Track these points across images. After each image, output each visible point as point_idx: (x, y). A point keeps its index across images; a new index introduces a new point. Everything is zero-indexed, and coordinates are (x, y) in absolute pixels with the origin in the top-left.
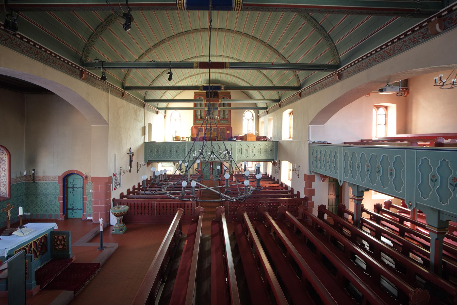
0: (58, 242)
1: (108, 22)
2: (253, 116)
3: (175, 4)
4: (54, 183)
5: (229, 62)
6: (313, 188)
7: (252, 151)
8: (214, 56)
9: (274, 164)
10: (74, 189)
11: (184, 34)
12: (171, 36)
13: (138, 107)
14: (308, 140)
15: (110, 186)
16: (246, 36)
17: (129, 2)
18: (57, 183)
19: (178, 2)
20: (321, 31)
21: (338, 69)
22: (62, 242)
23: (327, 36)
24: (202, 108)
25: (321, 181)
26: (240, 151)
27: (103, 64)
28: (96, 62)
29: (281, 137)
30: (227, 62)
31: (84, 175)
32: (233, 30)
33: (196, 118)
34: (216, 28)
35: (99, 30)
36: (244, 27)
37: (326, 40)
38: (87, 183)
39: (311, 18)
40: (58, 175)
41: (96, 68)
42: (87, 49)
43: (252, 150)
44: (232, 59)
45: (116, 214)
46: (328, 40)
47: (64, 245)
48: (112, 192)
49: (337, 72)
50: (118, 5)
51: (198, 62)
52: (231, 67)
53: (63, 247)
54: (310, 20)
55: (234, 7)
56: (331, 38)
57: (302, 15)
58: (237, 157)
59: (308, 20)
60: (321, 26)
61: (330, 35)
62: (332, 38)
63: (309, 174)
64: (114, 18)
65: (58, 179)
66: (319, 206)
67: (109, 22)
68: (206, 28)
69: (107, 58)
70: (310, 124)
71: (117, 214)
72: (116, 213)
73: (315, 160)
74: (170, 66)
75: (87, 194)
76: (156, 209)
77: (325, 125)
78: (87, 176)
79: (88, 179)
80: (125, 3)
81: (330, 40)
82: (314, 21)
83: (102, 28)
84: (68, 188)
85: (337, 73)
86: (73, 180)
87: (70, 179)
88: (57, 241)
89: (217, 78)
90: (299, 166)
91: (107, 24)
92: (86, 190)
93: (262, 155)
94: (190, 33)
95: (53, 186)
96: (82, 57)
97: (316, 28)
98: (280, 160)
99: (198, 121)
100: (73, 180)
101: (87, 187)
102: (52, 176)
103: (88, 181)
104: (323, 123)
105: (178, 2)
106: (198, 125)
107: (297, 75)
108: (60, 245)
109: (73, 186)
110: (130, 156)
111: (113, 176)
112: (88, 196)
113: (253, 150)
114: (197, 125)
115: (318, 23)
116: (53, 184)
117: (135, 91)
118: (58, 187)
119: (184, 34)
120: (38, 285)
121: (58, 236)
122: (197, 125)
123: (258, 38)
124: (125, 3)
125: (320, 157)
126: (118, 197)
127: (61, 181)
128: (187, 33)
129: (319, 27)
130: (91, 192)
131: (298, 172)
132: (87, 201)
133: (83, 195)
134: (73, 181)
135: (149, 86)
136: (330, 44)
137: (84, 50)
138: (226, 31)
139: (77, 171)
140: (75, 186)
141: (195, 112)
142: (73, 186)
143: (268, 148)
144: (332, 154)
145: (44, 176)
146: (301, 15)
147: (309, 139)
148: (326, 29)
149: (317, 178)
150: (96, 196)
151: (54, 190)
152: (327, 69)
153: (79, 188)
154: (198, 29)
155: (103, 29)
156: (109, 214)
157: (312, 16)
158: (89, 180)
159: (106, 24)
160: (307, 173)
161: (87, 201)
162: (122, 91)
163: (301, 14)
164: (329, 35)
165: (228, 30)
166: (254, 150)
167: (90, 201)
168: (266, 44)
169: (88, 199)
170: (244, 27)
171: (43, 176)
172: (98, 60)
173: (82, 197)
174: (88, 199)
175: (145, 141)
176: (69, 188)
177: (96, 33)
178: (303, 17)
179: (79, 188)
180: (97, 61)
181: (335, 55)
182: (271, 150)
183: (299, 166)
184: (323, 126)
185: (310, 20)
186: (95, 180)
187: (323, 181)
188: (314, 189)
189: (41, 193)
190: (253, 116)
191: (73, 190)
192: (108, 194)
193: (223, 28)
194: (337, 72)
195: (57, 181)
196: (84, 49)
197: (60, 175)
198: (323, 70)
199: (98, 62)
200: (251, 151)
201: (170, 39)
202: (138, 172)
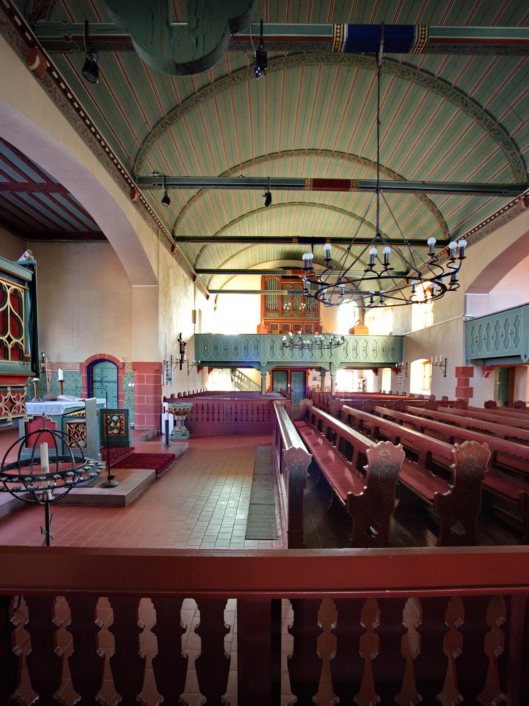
0: (112, 425)
1: (170, 118)
2: (354, 312)
3: (331, 38)
4: (74, 373)
5: (358, 180)
6: (470, 386)
7: (363, 349)
8: (303, 205)
9: (396, 370)
10: (104, 383)
11: (268, 158)
12: (247, 161)
13: (188, 278)
14: (464, 316)
15: (161, 376)
16: (363, 163)
17: (266, 34)
18: (78, 373)
19: (335, 35)
20: (499, 134)
21: (524, 191)
22: (118, 425)
23: (508, 142)
24: (276, 290)
25: (483, 376)
26: (344, 349)
27: (165, 178)
28: (155, 176)
29: (409, 327)
30: (355, 180)
31: (119, 362)
32: (344, 153)
33: (266, 309)
34: (318, 150)
35: (158, 130)
36: (364, 146)
37: (506, 149)
38: (124, 374)
39: (485, 114)
40: (80, 362)
41: (154, 185)
42: (140, 156)
43: (364, 348)
44: (332, 209)
45: (176, 411)
46: (510, 148)
47: (120, 429)
48: (163, 387)
49: (522, 196)
50: (248, 38)
51: (311, 179)
52: (361, 187)
53: (120, 432)
54: (482, 118)
55: (414, 46)
56: (516, 143)
57: (470, 110)
58: (340, 358)
59: (478, 118)
60: (500, 124)
61: (515, 139)
62: (517, 143)
63: (465, 366)
64: (180, 113)
65: (80, 367)
66: (486, 402)
67: (172, 118)
68: (302, 150)
69: (173, 172)
70: (467, 291)
71: (179, 411)
72: (176, 409)
73: (477, 342)
74: (268, 183)
75: (124, 389)
76: (231, 413)
77: (490, 293)
78: (123, 363)
79: (126, 368)
80: (259, 35)
81: (514, 146)
82: (489, 117)
83: (162, 127)
84: (93, 382)
85: (523, 197)
86: (102, 371)
87: (97, 370)
88: (111, 422)
89: (299, 250)
90: (446, 359)
91: (170, 122)
92: (124, 385)
93: (379, 355)
94: (276, 158)
95: (73, 377)
96: (133, 167)
97: (491, 131)
98: (407, 363)
99: (270, 314)
100: (102, 371)
101: (125, 379)
102: (71, 363)
103: (126, 371)
104: (487, 290)
105: (335, 35)
106: (270, 320)
107: (445, 222)
108: (114, 428)
109: (102, 379)
110: (181, 345)
111: (164, 364)
112: (126, 393)
113: (365, 349)
114: (268, 320)
115: (495, 119)
116: (72, 374)
117: (191, 243)
118: (80, 378)
119: (266, 159)
120: (104, 461)
121: (112, 415)
122: (268, 320)
123: (384, 165)
124: (259, 35)
125: (486, 333)
126: (169, 397)
127: (85, 370)
128: (271, 157)
129: (496, 128)
130: (130, 387)
131: (443, 368)
132: (124, 399)
133: (118, 391)
134: (101, 372)
135: (214, 236)
136: (512, 155)
137: (137, 157)
138: (333, 155)
139: (108, 355)
140: (105, 379)
141: (264, 299)
142: (102, 379)
143: (389, 345)
144: (510, 322)
145: (59, 363)
146: (468, 111)
147: (465, 314)
148: (508, 129)
149: (477, 372)
150: (141, 390)
151: (73, 383)
152: (508, 192)
153: (111, 382)
154: (289, 151)
155: (162, 129)
156: (159, 416)
157: (486, 110)
158: (128, 370)
159: (167, 121)
160: (461, 363)
161: (124, 399)
162: (173, 243)
163: (468, 109)
164: (512, 139)
165: (337, 153)
166: (366, 348)
167: (129, 399)
168: (396, 175)
169: (125, 397)
170: (364, 146)
171: (57, 363)
172: (157, 173)
173: (116, 396)
174: (126, 398)
175: (196, 333)
176: (95, 381)
177: (153, 134)
178: (470, 114)
179: (111, 382)
180: (156, 175)
181: (519, 171)
182: (393, 349)
183: (446, 359)
184: (487, 295)
185: (482, 118)
186: (137, 366)
187: (487, 376)
188: (472, 389)
189: (55, 388)
190: (354, 312)
191: (102, 385)
192: (158, 389)
193: (328, 149)
194: (522, 196)
195: (79, 371)
196: (137, 156)
197: (83, 361)
198: (502, 192)
199: (158, 176)
200: (362, 349)
201: (245, 167)
202: (188, 375)
